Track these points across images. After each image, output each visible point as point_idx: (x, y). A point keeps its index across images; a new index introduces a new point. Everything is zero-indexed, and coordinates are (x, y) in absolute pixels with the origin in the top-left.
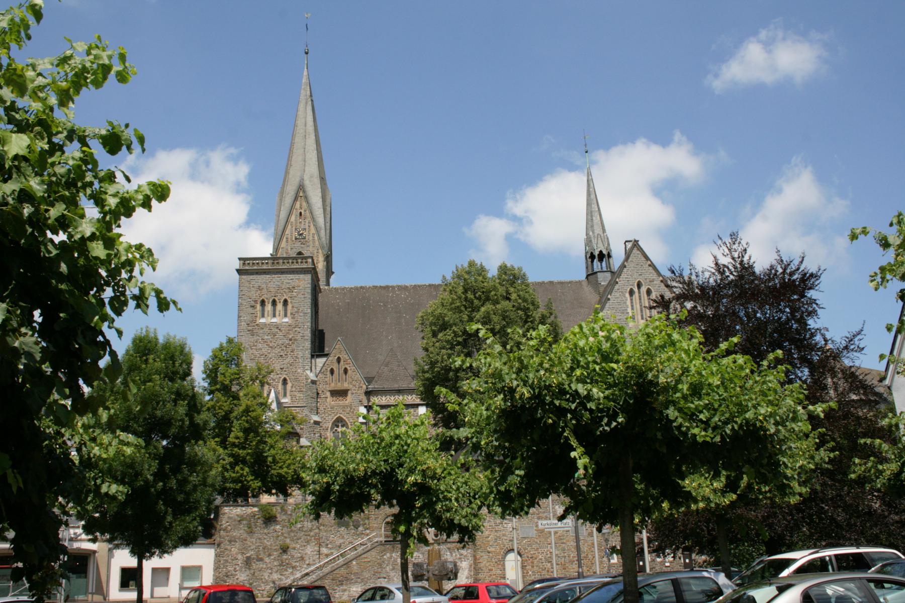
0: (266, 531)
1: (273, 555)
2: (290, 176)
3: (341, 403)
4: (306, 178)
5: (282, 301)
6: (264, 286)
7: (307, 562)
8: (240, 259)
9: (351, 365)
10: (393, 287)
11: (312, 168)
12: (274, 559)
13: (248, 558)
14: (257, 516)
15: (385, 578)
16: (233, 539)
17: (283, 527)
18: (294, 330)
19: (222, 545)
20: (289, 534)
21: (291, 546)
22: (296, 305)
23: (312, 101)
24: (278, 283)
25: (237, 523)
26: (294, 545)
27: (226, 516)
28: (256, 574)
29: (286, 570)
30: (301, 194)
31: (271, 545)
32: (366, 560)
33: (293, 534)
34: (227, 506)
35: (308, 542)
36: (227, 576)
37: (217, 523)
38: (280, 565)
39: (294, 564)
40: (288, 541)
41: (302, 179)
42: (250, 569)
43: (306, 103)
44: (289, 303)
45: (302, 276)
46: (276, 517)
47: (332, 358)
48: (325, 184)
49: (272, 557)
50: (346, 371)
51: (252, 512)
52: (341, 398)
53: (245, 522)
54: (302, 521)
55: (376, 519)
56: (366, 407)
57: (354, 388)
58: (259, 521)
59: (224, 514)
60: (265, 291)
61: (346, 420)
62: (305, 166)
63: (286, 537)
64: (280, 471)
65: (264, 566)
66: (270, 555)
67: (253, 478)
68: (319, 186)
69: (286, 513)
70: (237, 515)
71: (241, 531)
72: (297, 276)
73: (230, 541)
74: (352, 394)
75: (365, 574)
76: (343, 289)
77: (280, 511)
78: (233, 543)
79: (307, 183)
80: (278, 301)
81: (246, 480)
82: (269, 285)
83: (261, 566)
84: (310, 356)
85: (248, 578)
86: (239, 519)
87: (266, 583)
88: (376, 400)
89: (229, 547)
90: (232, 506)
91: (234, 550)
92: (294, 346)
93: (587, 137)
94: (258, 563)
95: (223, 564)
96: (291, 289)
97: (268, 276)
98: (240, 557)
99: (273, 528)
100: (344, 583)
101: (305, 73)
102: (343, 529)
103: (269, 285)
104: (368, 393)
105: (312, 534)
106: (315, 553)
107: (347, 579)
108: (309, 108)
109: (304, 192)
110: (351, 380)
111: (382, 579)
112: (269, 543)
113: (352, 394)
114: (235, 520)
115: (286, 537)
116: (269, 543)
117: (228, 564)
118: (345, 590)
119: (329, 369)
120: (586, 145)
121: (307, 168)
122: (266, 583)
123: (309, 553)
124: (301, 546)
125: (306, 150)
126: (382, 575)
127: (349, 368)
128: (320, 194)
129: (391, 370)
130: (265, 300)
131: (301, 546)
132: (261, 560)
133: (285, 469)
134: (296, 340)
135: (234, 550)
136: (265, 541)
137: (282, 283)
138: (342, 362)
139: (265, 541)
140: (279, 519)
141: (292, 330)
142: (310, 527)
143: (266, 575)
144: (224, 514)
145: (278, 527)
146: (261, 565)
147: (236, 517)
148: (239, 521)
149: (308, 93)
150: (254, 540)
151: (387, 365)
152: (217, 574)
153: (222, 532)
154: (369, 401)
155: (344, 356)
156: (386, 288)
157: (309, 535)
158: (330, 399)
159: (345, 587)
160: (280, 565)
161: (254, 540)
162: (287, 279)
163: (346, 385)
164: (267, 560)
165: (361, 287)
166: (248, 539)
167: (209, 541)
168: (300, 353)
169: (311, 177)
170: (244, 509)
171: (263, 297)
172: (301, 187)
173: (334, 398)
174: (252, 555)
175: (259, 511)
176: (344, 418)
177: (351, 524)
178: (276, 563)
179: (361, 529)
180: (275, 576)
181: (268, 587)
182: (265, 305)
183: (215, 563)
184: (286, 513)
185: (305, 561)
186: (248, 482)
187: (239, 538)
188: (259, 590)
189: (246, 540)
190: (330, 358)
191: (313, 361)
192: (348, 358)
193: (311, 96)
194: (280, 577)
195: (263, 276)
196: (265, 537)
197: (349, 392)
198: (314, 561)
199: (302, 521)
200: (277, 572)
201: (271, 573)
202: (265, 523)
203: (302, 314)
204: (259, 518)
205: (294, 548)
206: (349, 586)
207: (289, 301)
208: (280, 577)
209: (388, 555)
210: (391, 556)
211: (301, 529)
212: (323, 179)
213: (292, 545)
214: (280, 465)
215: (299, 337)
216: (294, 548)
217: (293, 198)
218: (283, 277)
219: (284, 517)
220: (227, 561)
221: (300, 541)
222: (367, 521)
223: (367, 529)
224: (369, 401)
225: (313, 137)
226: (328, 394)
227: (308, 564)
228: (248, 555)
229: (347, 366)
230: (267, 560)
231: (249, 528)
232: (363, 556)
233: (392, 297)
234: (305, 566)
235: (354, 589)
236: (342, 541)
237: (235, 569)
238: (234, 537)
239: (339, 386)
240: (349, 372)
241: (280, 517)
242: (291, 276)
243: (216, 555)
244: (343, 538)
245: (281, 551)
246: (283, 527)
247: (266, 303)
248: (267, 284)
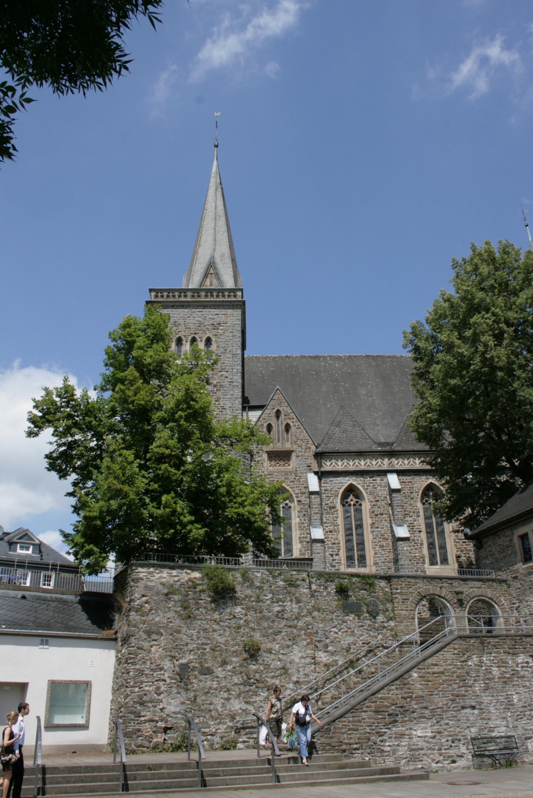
0: (216, 616)
1: (231, 661)
2: (199, 255)
3: (282, 468)
4: (216, 256)
5: (204, 339)
6: (181, 321)
7: (294, 679)
8: (151, 290)
9: (295, 419)
10: (324, 357)
11: (224, 248)
12: (234, 672)
13: (184, 667)
14: (199, 588)
15: (473, 708)
16: (154, 629)
17: (248, 609)
18: (220, 374)
19: (133, 640)
20: (259, 624)
21: (263, 646)
22: (222, 345)
23: (222, 188)
24: (199, 319)
25: (163, 598)
26: (269, 645)
27: (141, 584)
28: (199, 700)
29: (256, 694)
30: (212, 271)
31: (227, 643)
32: (436, 669)
33: (266, 624)
34: (142, 566)
35: (294, 639)
36: (142, 704)
37: (124, 596)
38: (244, 684)
39: (271, 681)
40: (257, 636)
41: (213, 257)
42: (187, 690)
43: (216, 189)
44: (213, 343)
45: (229, 311)
46: (233, 590)
47: (270, 411)
48: (236, 263)
49: (229, 667)
50: (288, 427)
51: (190, 580)
52: (282, 463)
53: (176, 597)
54: (280, 600)
55: (405, 600)
56: (316, 473)
57: (300, 449)
58: (203, 596)
59: (137, 580)
60: (182, 328)
61: (290, 490)
62: (215, 245)
63: (253, 630)
64: (241, 510)
65: (215, 685)
66: (224, 663)
67: (193, 518)
68: (231, 266)
69: (252, 585)
70: (163, 584)
71: (171, 614)
72: (223, 311)
73: (149, 633)
74: (298, 456)
75: (436, 699)
76: (266, 358)
77: (240, 579)
78: (154, 637)
79: (218, 260)
80: (199, 339)
81: (181, 523)
82: (187, 321)
83: (209, 683)
84: (241, 406)
85: (183, 707)
86: (166, 591)
87: (219, 718)
88: (328, 465)
89: (146, 645)
90: (153, 566)
91: (156, 652)
92: (219, 394)
93: (525, 211)
94: (202, 677)
95: (134, 678)
96: (215, 326)
97: (186, 310)
98: (167, 664)
99: (228, 610)
100: (399, 718)
101: (215, 163)
102: (351, 617)
103: (187, 321)
104: (319, 456)
105: (300, 624)
106: (308, 660)
107: (405, 711)
108: (220, 197)
109: (215, 268)
110: (294, 439)
111: (468, 711)
112: (222, 640)
113: (298, 456)
114: (158, 593)
115: (253, 630)
116: (222, 640)
117: (144, 679)
118: (402, 735)
119: (265, 425)
120: (525, 219)
121: (217, 247)
122: (219, 718)
123: (297, 660)
124: (282, 647)
125: (217, 230)
126: (469, 702)
127: (292, 424)
128: (232, 274)
129: (345, 431)
130: (183, 337)
131: (282, 647)
132: (208, 672)
133: (248, 508)
134: (222, 386)
135: (156, 652)
136: (216, 635)
137: (205, 318)
138: (282, 417)
139: (216, 635)
140: (239, 594)
141: (217, 374)
142: (296, 610)
143: (218, 702)
144: (137, 580)
145: (238, 609)
146: (209, 682)
147: (161, 587)
148: (167, 595)
149: (218, 181)
150: (194, 632)
151: (338, 426)
152: (121, 700)
153: (133, 613)
154: (320, 466)
155: (285, 409)
156: (317, 357)
157: (295, 627)
158: (266, 463)
159: (399, 729)
160: (244, 684)
161: (194, 632)
162: (211, 314)
163: (288, 446)
164: (219, 672)
165: (287, 357)
166: (184, 630)
167: (106, 633)
168: (228, 402)
169: (223, 256)
170: (174, 572)
171: (180, 335)
172: (211, 265)
173: (273, 463)
174: (190, 662)
175: (202, 579)
176: (288, 488)
177: (364, 609)
178: (236, 680)
179: (380, 618)
180: (236, 705)
181: (223, 727)
182: (182, 344)
183: (116, 677)
184: (252, 585)
185: (290, 675)
186: (184, 526)
187: (166, 628)
188: (204, 734)
189: (179, 632)
190: (267, 411)
191: (244, 414)
192: (290, 411)
193: (221, 184)
194: (245, 706)
195: (180, 310)
196: (216, 627)
197: (293, 454)
198: (307, 675)
199: (280, 600)
200: (239, 696)
201: (228, 699)
202: (214, 601)
203: (229, 356)
204: (203, 591)
205: (270, 651)
206: (409, 725)
207: (213, 339)
208: (245, 706)
209: (475, 659)
210: (481, 662)
211: (280, 615)
212: (233, 260)
213: (266, 645)
214: (239, 500)
215: (226, 383)
216: (270, 651)
217: (203, 276)
218: (206, 311)
219: (249, 592)
220: (141, 672)
221: (279, 637)
222: (389, 606)
223: (391, 619)
224: (320, 466)
225: (223, 219)
226: (265, 456)
227: (297, 682)
228: (184, 661)
229: (289, 422)
230: (219, 672)
231: (185, 608)
232: (430, 661)
233: (325, 366)
234: (291, 686)
235: (419, 733)
236: (350, 639)
237: (158, 688)
238: (156, 624)
239: (278, 446)
240: (293, 429)
241: (241, 591)
242: (216, 311)
243: (119, 661)
244: (353, 634)
245: (245, 655)
246: (248, 609)
247: (184, 342)
248: (184, 318)
